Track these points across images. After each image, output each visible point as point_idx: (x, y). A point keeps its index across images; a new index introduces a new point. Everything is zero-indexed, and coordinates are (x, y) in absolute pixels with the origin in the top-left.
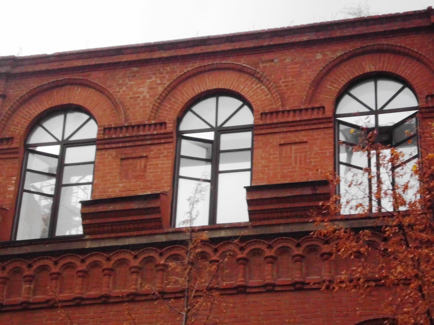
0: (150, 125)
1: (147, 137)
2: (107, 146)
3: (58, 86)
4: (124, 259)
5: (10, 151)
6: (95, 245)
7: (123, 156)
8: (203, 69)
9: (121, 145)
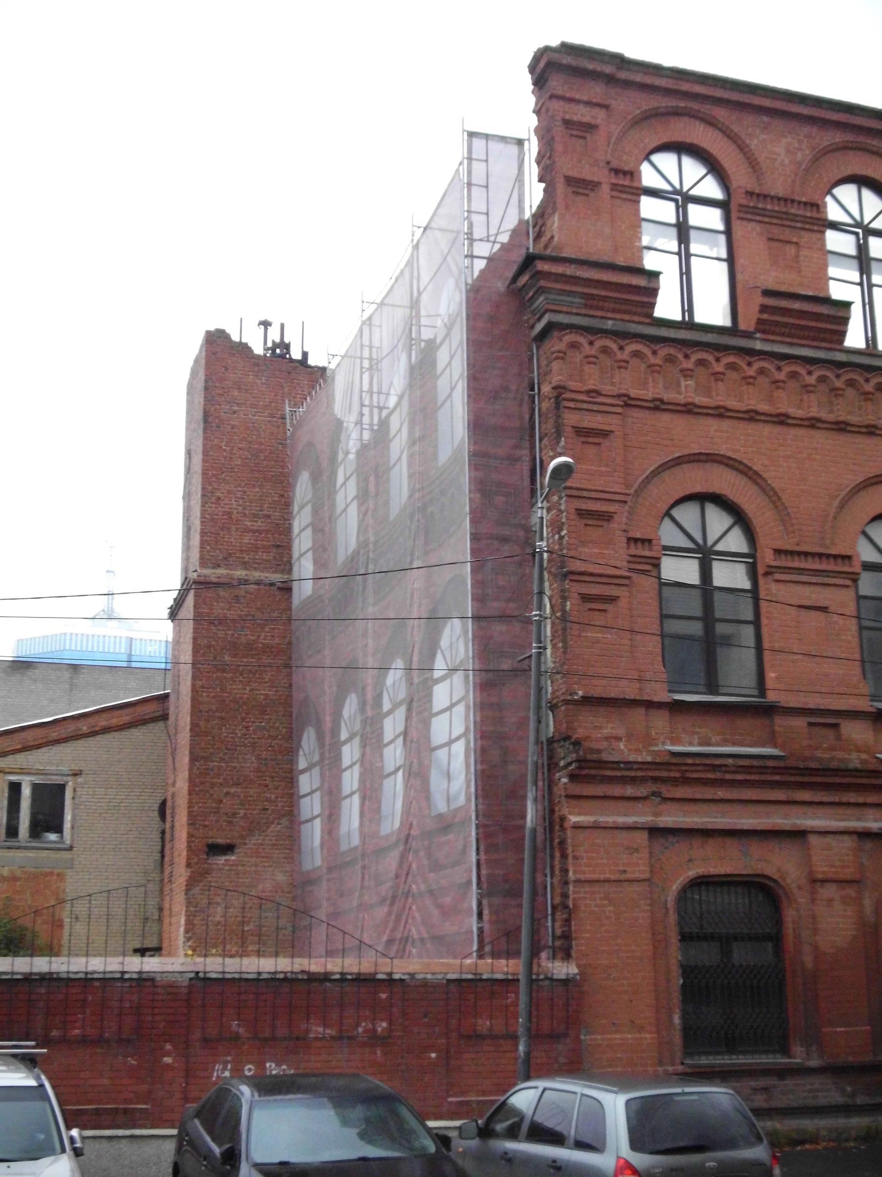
0: (799, 202)
1: (798, 218)
2: (750, 216)
3: (676, 113)
4: (705, 360)
5: (631, 190)
6: (767, 347)
7: (770, 236)
8: (850, 145)
9: (766, 220)
